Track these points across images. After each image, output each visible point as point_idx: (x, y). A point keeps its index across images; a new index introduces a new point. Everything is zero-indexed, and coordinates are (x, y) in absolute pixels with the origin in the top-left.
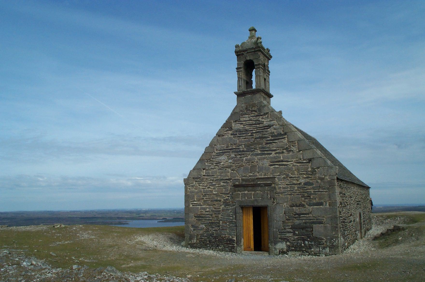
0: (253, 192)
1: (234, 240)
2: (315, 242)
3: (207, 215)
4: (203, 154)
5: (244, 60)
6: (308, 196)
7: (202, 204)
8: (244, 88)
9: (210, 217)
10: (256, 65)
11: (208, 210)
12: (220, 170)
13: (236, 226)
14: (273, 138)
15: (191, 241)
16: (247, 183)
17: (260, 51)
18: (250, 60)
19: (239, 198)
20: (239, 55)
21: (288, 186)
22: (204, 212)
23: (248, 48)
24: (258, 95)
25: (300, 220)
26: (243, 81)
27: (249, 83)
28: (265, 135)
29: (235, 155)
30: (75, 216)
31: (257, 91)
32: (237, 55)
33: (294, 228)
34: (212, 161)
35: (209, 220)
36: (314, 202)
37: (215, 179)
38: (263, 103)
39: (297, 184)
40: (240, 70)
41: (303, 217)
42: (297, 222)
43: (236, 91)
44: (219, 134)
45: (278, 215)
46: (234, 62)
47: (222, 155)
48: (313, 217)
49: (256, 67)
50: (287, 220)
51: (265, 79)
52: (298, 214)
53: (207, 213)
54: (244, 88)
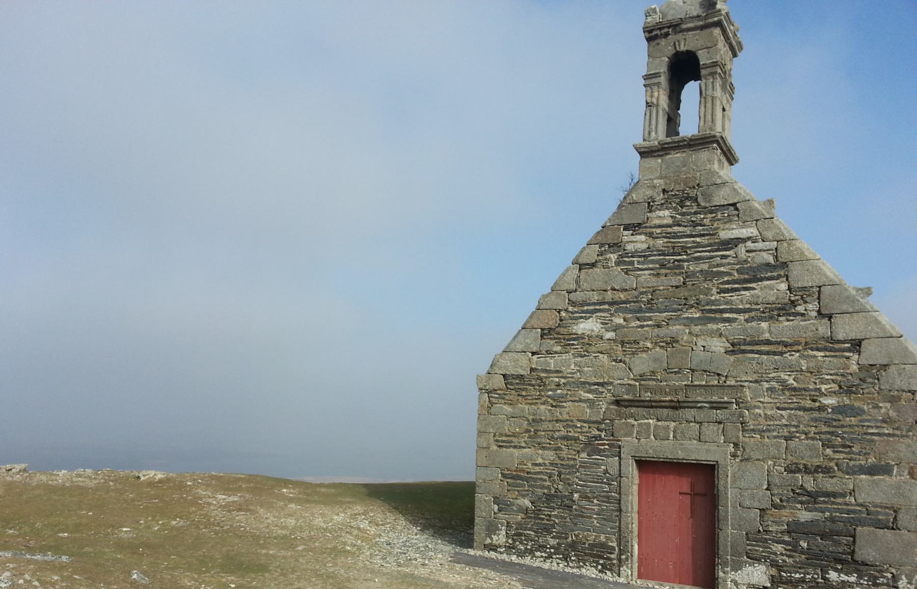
0: (673, 424)
1: (613, 548)
2: (860, 577)
3: (539, 473)
4: (533, 313)
5: (670, 51)
6: (845, 446)
7: (523, 444)
8: (660, 135)
9: (545, 480)
10: (706, 66)
11: (540, 461)
12: (580, 359)
13: (620, 510)
14: (742, 277)
15: (492, 539)
16: (657, 398)
17: (719, 24)
18: (688, 51)
19: (631, 435)
20: (656, 37)
21: (783, 413)
22: (530, 465)
23: (682, 16)
24: (704, 155)
25: (816, 510)
26: (661, 112)
27: (672, 121)
28: (718, 266)
29: (625, 320)
30: (86, 477)
31: (703, 142)
32: (649, 40)
33: (795, 529)
34: (558, 333)
35: (543, 487)
36: (863, 463)
37: (563, 381)
38: (720, 177)
39: (811, 409)
40: (656, 81)
41: (824, 502)
42: (805, 516)
43: (639, 141)
44: (580, 261)
45: (744, 490)
46: (637, 59)
47: (586, 318)
48: (858, 505)
49: (703, 72)
50: (774, 506)
51: (724, 110)
52: (809, 494)
53: (537, 469)
54: (660, 135)
